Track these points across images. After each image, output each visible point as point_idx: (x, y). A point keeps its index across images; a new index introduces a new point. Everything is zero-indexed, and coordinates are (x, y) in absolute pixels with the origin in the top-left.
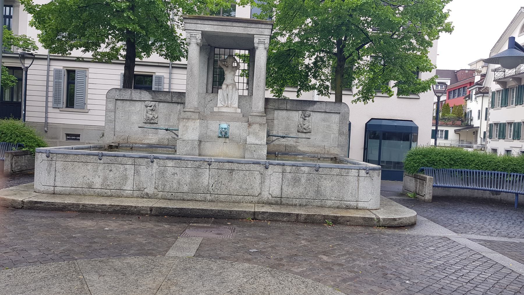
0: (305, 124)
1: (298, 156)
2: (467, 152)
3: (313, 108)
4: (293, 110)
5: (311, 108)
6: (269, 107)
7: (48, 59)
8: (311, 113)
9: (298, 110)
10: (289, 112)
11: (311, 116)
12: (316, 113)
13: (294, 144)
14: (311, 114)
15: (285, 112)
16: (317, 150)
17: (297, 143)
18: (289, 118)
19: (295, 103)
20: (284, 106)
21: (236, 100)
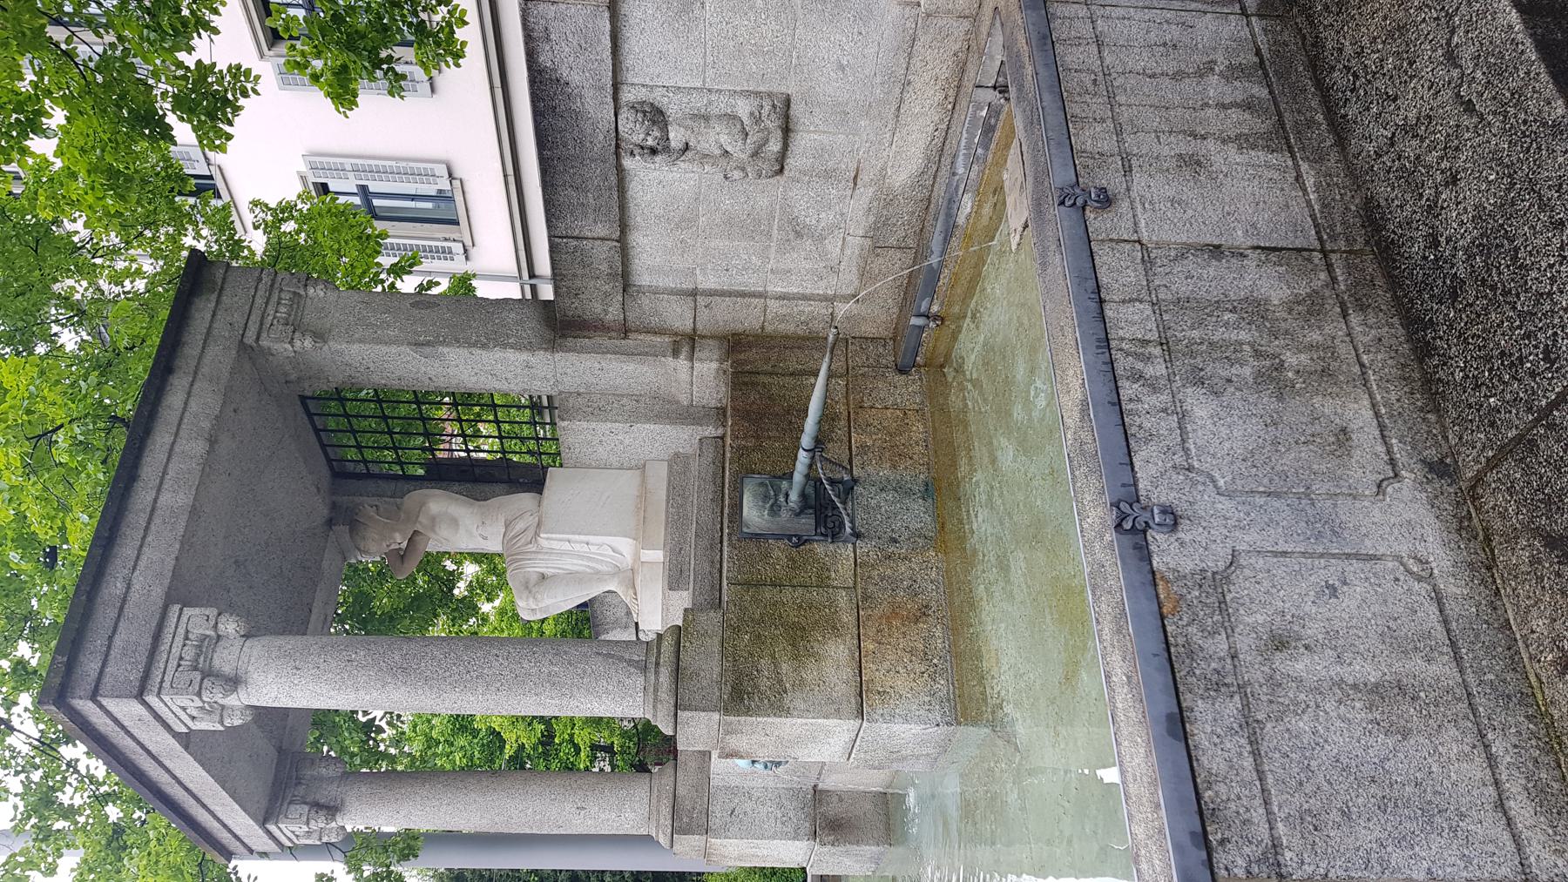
0: (717, 152)
1: (961, 220)
2: (88, 534)
3: (589, 94)
4: (623, 207)
5: (596, 108)
6: (613, 313)
7: (533, 281)
8: (628, 96)
9: (613, 179)
10: (637, 216)
11: (658, 97)
12: (628, 61)
13: (866, 194)
14: (643, 94)
15: (638, 239)
16: (934, 66)
17: (865, 177)
18: (683, 219)
19: (567, 195)
20: (602, 254)
21: (593, 549)
